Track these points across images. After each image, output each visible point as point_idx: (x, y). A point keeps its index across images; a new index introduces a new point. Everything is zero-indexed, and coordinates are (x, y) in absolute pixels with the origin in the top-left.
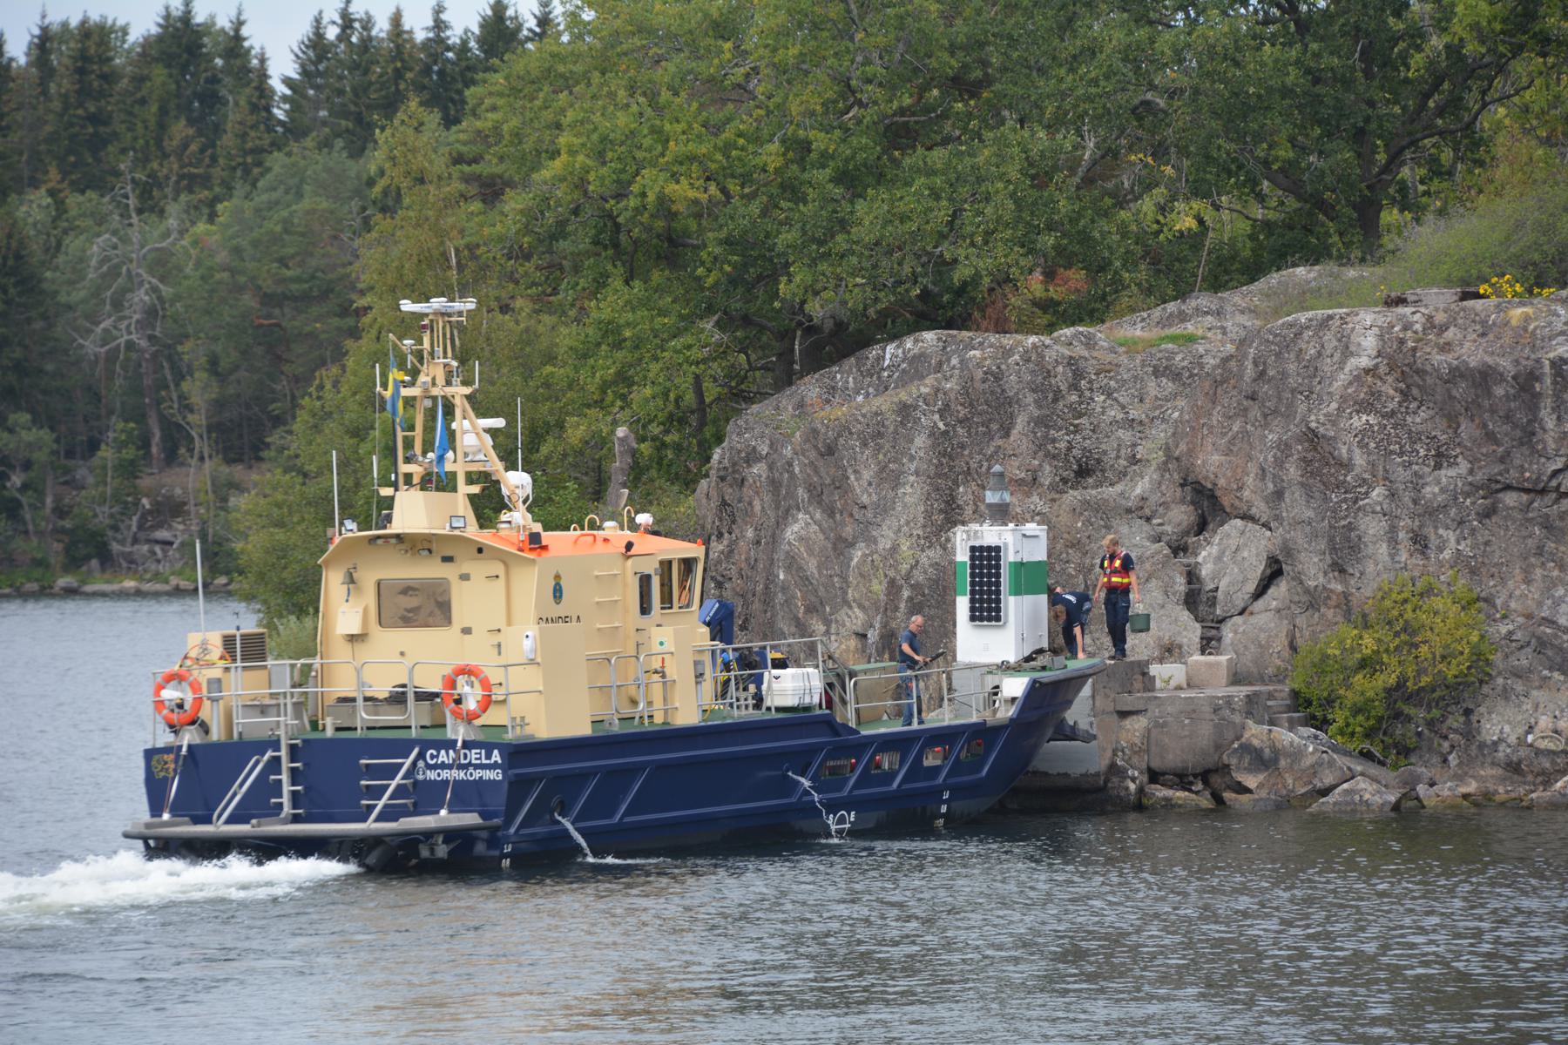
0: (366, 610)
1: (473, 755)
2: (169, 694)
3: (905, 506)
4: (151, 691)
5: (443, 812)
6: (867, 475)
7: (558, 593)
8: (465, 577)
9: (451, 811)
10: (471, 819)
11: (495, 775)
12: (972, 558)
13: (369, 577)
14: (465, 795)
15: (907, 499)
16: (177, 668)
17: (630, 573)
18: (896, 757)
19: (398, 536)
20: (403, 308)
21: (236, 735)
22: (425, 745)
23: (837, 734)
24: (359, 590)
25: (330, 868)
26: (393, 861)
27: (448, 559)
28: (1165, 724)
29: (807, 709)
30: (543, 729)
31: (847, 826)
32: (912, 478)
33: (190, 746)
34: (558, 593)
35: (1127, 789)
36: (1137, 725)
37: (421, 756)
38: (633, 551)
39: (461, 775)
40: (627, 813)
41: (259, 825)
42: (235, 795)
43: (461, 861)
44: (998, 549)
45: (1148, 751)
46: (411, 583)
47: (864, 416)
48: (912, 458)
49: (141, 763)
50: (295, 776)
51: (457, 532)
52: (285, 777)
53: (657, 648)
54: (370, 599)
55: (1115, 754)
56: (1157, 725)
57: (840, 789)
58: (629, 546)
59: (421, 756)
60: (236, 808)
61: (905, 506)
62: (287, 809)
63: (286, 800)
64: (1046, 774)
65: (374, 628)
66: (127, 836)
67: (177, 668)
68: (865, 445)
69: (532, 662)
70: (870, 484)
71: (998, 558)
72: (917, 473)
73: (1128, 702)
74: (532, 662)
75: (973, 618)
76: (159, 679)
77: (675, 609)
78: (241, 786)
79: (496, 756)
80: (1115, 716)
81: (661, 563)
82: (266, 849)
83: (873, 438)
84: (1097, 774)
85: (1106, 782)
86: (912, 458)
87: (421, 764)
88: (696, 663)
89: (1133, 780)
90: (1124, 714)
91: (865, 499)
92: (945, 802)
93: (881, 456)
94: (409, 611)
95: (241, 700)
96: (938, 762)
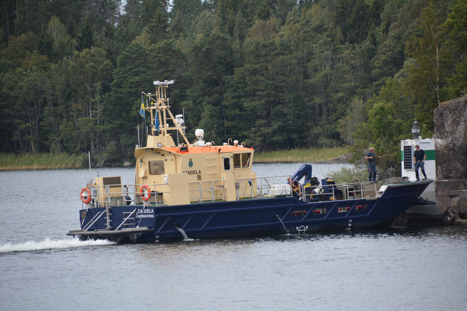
0: (146, 170)
1: (148, 211)
2: (84, 194)
3: (459, 132)
4: (80, 193)
5: (137, 227)
6: (449, 122)
7: (191, 164)
8: (166, 160)
9: (139, 227)
10: (145, 228)
11: (152, 216)
12: (405, 150)
13: (147, 160)
14: (144, 222)
15: (460, 130)
16: (85, 187)
17: (220, 158)
18: (325, 210)
19: (149, 149)
20: (154, 84)
21: (98, 206)
22: (138, 208)
23: (297, 203)
24: (144, 164)
25: (105, 242)
26: (124, 240)
27: (163, 155)
28: (465, 199)
29: (285, 196)
30: (170, 201)
31: (305, 230)
32: (463, 123)
33: (89, 209)
34: (191, 164)
35: (447, 219)
36: (456, 199)
37: (137, 211)
38: (221, 152)
39: (144, 216)
40: (207, 226)
41: (97, 231)
42: (91, 222)
43: (145, 239)
44: (410, 147)
45: (459, 207)
46: (156, 162)
47: (455, 103)
48: (464, 116)
49: (79, 214)
50: (111, 217)
51: (159, 148)
52: (107, 217)
53: (222, 179)
54: (147, 167)
55: (448, 208)
56: (462, 200)
57: (301, 219)
58: (220, 150)
59: (137, 211)
60: (91, 227)
61: (459, 132)
62: (109, 226)
63: (108, 224)
64: (427, 215)
65: (149, 175)
66: (68, 235)
67: (85, 187)
68: (450, 113)
69: (167, 184)
70: (450, 125)
71: (411, 150)
72: (464, 121)
73: (453, 192)
74: (167, 184)
75: (405, 168)
76: (81, 191)
77: (241, 168)
78: (94, 220)
79: (152, 211)
80: (449, 197)
81: (234, 155)
82: (96, 237)
83: (454, 110)
84: (440, 215)
85: (443, 217)
86: (464, 116)
87: (137, 213)
88: (236, 184)
89: (450, 217)
90: (452, 197)
91: (448, 130)
92: (350, 223)
93: (454, 116)
94: (156, 170)
95: (104, 196)
96: (345, 211)
